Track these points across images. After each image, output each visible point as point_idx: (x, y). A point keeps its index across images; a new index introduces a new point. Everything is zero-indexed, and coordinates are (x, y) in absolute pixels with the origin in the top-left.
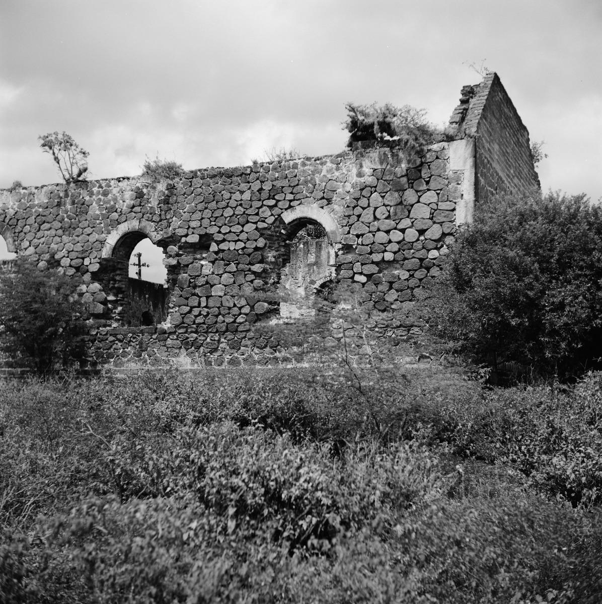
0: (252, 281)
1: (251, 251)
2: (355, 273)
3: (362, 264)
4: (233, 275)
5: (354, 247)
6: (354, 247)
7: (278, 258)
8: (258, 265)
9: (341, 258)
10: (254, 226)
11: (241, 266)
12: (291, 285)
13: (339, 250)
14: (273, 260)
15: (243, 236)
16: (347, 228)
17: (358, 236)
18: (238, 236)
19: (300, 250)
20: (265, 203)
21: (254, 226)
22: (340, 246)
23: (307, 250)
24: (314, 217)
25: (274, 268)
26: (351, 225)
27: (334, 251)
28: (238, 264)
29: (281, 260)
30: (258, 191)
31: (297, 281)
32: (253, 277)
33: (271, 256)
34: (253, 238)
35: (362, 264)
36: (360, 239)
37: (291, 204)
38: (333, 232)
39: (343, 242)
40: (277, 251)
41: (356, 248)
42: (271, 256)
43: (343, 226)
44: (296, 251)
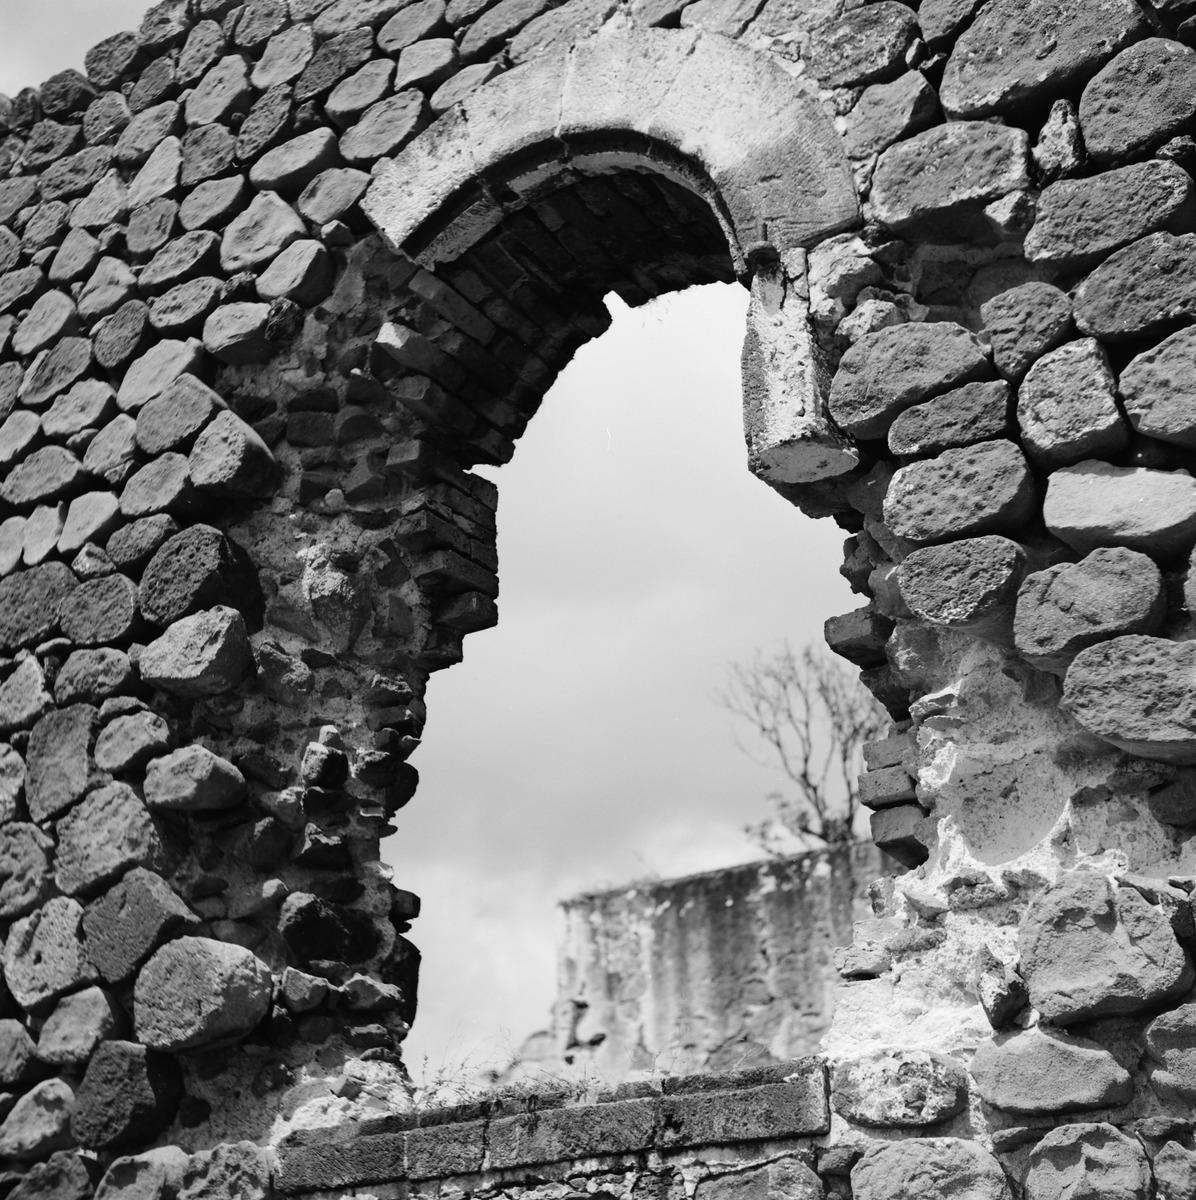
0: (134, 772)
1: (144, 533)
2: (1041, 466)
3: (1117, 352)
4: (21, 747)
5: (1000, 213)
6: (1000, 213)
7: (389, 577)
8: (191, 622)
9: (879, 356)
10: (184, 351)
11: (79, 664)
12: (791, 1041)
13: (849, 292)
14: (333, 580)
15: (109, 450)
16: (913, 83)
17: (1025, 110)
18: (80, 451)
19: (818, 888)
20: (258, 172)
21: (184, 351)
22: (856, 253)
23: (845, 885)
24: (603, 112)
25: (347, 657)
26: (945, 44)
27: (795, 312)
28: (61, 654)
29: (410, 593)
30: (221, 120)
31: (816, 1022)
32: (143, 728)
33: (311, 563)
34: (169, 435)
35: (1117, 352)
36: (1057, 128)
37: (436, 100)
38: (779, 166)
39: (880, 211)
40: (366, 522)
41: (1023, 217)
42: (311, 563)
43: (861, 84)
44: (801, 892)
